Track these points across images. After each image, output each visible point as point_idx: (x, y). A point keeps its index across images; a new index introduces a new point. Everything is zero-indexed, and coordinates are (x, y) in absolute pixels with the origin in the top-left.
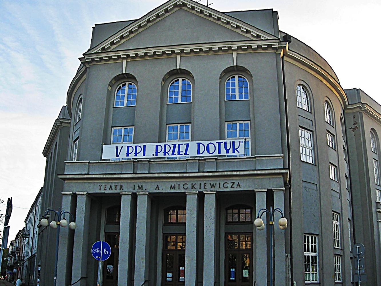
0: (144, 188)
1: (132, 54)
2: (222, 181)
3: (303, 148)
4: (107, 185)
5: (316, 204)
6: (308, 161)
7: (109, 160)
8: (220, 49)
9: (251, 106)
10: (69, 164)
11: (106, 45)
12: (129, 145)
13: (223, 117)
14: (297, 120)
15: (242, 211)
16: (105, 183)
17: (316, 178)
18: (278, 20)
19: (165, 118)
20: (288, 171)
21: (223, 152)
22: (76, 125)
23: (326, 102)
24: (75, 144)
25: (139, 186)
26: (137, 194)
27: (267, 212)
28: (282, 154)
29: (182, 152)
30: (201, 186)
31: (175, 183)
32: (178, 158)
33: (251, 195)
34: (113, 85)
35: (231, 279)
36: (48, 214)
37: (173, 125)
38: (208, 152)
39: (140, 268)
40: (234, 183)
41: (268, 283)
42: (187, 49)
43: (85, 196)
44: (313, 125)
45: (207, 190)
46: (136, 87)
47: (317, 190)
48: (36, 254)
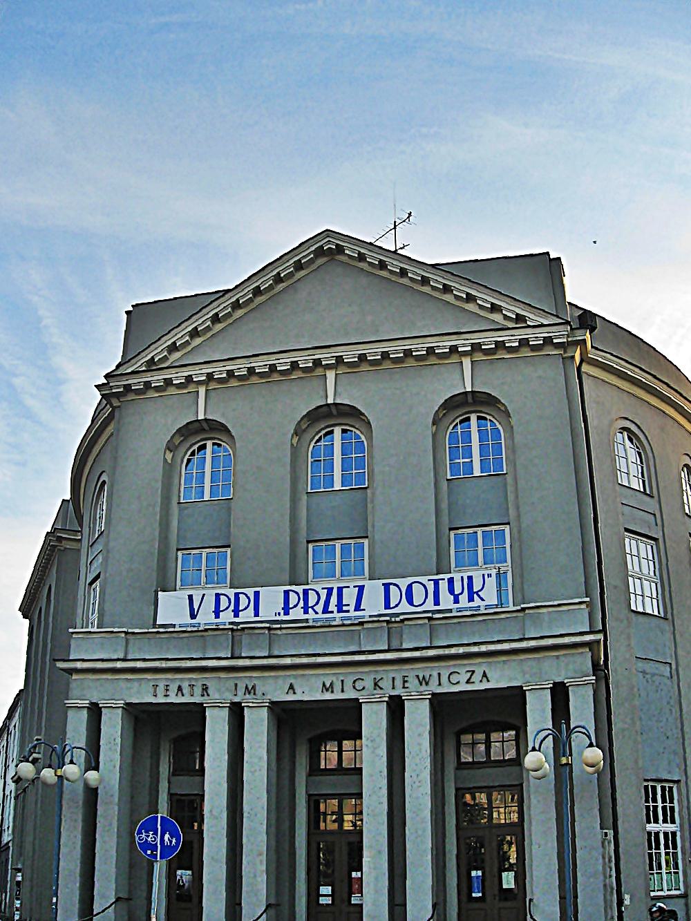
0: (259, 691)
2: (445, 669)
4: (171, 686)
5: (671, 710)
7: (174, 626)
8: (230, 374)
9: (510, 489)
10: (80, 636)
11: (157, 351)
12: (219, 591)
14: (620, 516)
15: (495, 736)
18: (564, 278)
19: (303, 523)
20: (600, 637)
21: (446, 601)
22: (95, 545)
23: (685, 469)
24: (92, 590)
25: (247, 688)
26: (243, 705)
27: (553, 736)
28: (587, 597)
29: (348, 605)
31: (334, 679)
32: (337, 619)
33: (514, 699)
34: (177, 447)
35: (474, 895)
36: (37, 751)
37: (323, 544)
38: (410, 602)
41: (562, 900)
42: (350, 355)
43: (121, 709)
44: (657, 525)
45: (410, 692)
46: (231, 452)
47: (672, 677)
48: (10, 844)
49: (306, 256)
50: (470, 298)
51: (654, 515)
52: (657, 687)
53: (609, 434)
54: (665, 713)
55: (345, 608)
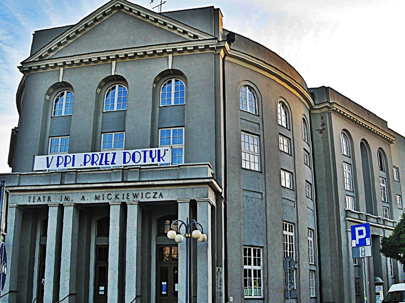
1: (68, 61)
2: (144, 191)
3: (251, 155)
6: (253, 168)
13: (157, 124)
16: (34, 194)
17: (262, 186)
29: (109, 161)
30: (124, 197)
34: (103, 87)
38: (134, 161)
39: (65, 281)
42: (121, 54)
43: (15, 208)
44: (260, 129)
46: (127, 90)
47: (262, 199)
50: (175, 28)
51: (259, 124)
52: (254, 203)
53: (237, 88)
54: (257, 216)
55: (108, 163)
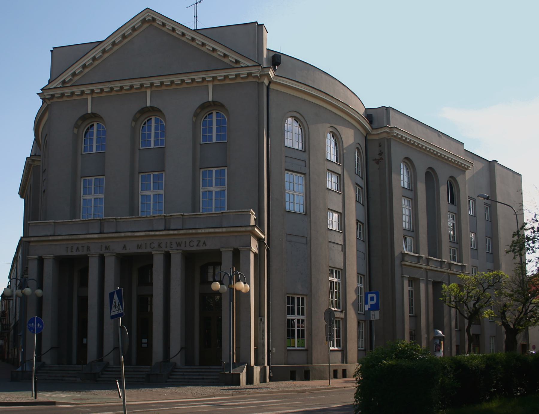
40: (199, 241)
49: (137, 23)
51: (305, 161)
